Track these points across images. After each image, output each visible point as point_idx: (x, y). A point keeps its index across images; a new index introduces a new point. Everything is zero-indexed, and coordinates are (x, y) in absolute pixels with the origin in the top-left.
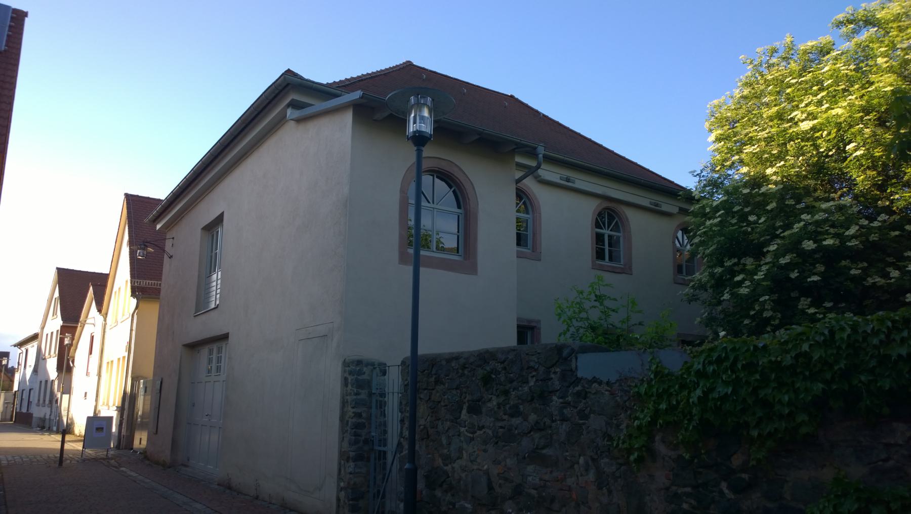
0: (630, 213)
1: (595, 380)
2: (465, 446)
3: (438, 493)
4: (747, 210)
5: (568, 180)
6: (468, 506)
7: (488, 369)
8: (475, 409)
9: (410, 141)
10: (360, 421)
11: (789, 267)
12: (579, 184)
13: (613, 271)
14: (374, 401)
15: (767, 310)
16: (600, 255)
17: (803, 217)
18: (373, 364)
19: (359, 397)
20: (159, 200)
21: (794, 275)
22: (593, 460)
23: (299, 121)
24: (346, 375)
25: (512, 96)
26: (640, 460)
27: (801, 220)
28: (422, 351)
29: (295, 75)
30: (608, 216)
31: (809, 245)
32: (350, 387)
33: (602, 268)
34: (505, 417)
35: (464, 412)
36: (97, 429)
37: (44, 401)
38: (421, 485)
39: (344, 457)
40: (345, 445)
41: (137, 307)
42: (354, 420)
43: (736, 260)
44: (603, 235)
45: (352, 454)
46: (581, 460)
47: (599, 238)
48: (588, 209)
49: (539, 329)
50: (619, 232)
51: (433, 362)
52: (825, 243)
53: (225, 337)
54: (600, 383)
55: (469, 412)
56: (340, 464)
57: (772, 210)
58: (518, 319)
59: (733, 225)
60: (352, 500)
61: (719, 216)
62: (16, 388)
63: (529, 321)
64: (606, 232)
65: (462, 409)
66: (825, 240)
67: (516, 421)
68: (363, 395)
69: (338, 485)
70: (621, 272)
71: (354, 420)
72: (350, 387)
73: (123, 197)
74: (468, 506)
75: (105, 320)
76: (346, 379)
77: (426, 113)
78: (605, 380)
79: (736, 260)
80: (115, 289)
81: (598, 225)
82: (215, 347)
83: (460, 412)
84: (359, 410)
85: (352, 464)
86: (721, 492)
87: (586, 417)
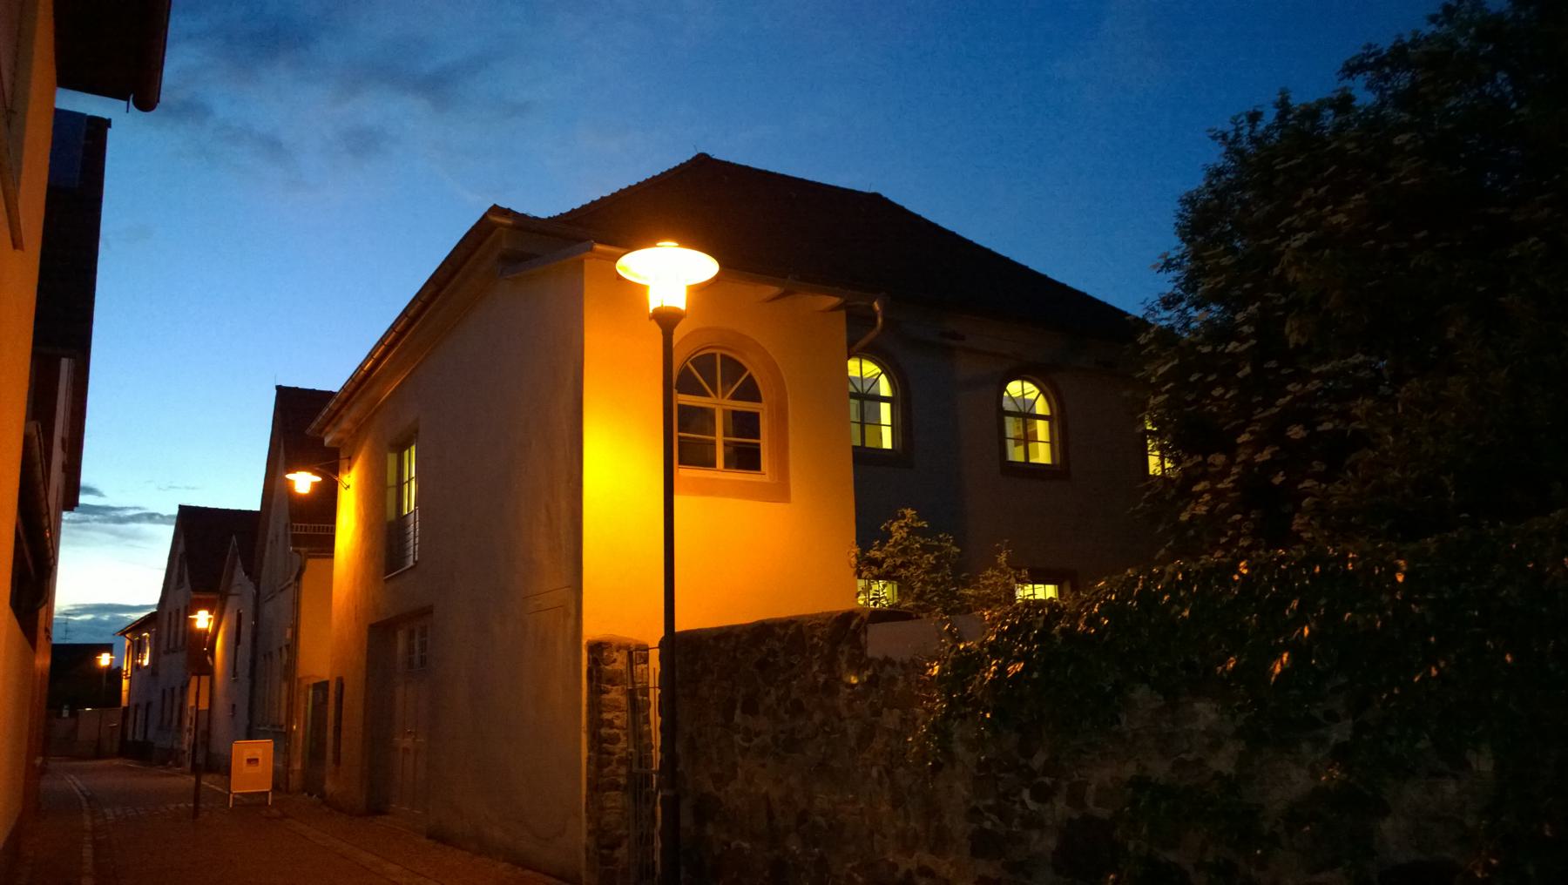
1: (888, 661)
2: (739, 759)
3: (710, 830)
4: (1210, 378)
6: (746, 845)
8: (751, 707)
9: (653, 322)
11: (1270, 467)
15: (1243, 535)
17: (1290, 387)
18: (627, 647)
20: (330, 394)
21: (1278, 480)
25: (876, 197)
26: (937, 767)
27: (1289, 393)
28: (680, 626)
29: (507, 212)
31: (1296, 432)
35: (738, 712)
36: (249, 761)
37: (180, 721)
38: (686, 821)
43: (1200, 458)
46: (874, 773)
52: (1320, 429)
53: (427, 612)
54: (893, 664)
55: (743, 712)
57: (1246, 377)
59: (1189, 404)
61: (1167, 391)
62: (124, 702)
66: (1321, 423)
73: (274, 392)
74: (746, 845)
75: (257, 587)
78: (898, 660)
79: (1200, 458)
80: (270, 537)
86: (1023, 803)
87: (878, 713)
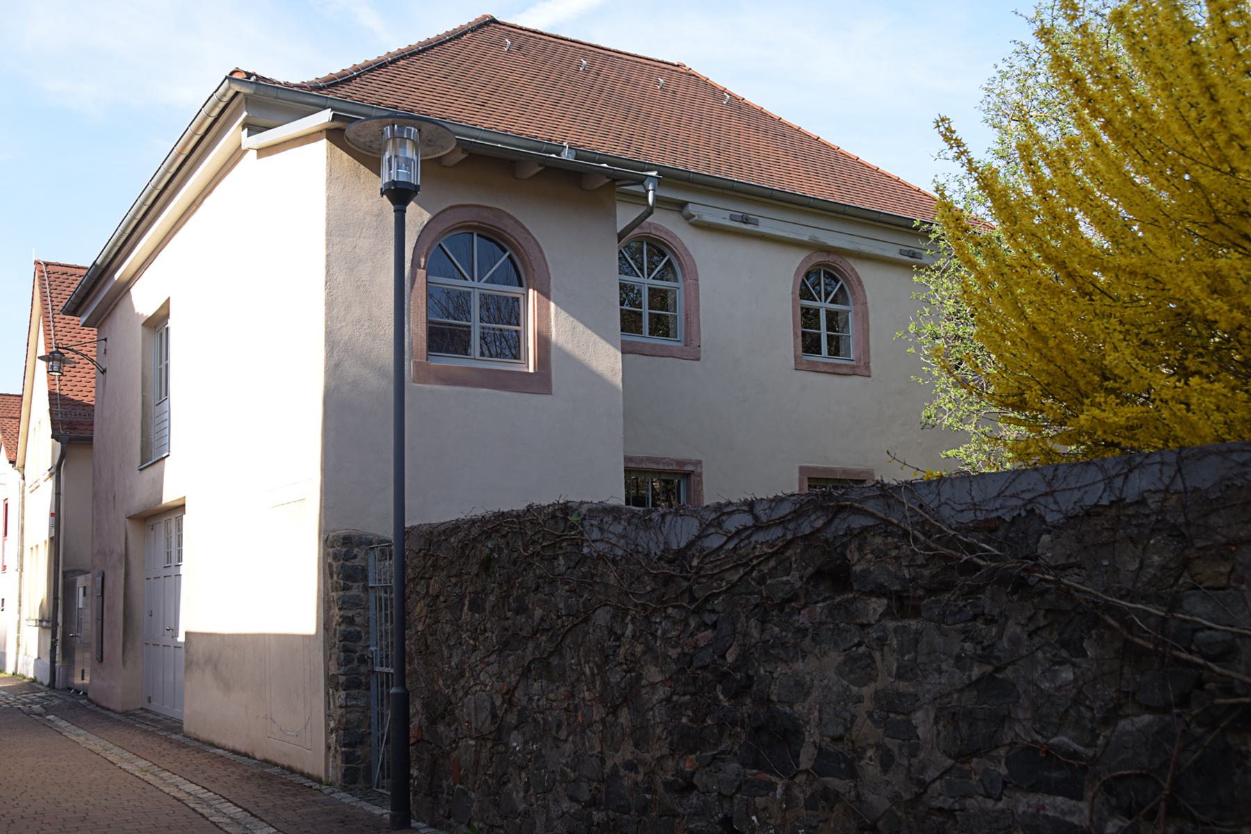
0: (868, 275)
5: (746, 221)
7: (490, 545)
10: (352, 629)
12: (765, 227)
13: (835, 371)
14: (372, 597)
16: (810, 345)
19: (348, 593)
22: (599, 667)
23: (263, 151)
24: (330, 560)
30: (825, 280)
32: (335, 577)
33: (814, 368)
34: (509, 614)
38: (417, 719)
39: (331, 682)
40: (334, 669)
41: (63, 456)
42: (343, 627)
44: (817, 312)
45: (342, 679)
47: (809, 317)
48: (784, 269)
49: (700, 475)
50: (846, 303)
51: (435, 537)
56: (327, 693)
58: (627, 459)
60: (345, 745)
63: (682, 463)
64: (823, 306)
65: (463, 605)
67: (522, 619)
68: (356, 590)
69: (327, 725)
70: (852, 372)
71: (343, 627)
72: (335, 577)
76: (330, 565)
77: (410, 152)
81: (805, 294)
82: (173, 517)
83: (462, 610)
84: (350, 614)
85: (342, 693)
